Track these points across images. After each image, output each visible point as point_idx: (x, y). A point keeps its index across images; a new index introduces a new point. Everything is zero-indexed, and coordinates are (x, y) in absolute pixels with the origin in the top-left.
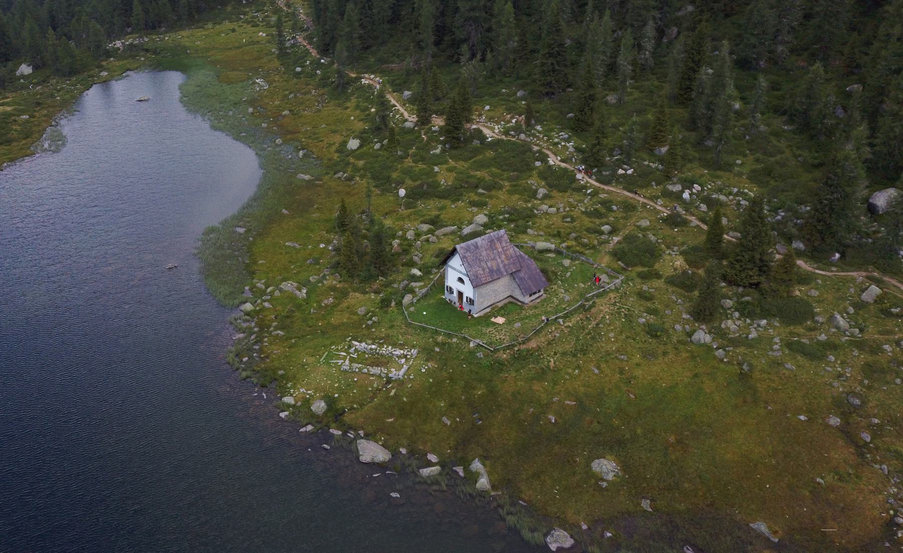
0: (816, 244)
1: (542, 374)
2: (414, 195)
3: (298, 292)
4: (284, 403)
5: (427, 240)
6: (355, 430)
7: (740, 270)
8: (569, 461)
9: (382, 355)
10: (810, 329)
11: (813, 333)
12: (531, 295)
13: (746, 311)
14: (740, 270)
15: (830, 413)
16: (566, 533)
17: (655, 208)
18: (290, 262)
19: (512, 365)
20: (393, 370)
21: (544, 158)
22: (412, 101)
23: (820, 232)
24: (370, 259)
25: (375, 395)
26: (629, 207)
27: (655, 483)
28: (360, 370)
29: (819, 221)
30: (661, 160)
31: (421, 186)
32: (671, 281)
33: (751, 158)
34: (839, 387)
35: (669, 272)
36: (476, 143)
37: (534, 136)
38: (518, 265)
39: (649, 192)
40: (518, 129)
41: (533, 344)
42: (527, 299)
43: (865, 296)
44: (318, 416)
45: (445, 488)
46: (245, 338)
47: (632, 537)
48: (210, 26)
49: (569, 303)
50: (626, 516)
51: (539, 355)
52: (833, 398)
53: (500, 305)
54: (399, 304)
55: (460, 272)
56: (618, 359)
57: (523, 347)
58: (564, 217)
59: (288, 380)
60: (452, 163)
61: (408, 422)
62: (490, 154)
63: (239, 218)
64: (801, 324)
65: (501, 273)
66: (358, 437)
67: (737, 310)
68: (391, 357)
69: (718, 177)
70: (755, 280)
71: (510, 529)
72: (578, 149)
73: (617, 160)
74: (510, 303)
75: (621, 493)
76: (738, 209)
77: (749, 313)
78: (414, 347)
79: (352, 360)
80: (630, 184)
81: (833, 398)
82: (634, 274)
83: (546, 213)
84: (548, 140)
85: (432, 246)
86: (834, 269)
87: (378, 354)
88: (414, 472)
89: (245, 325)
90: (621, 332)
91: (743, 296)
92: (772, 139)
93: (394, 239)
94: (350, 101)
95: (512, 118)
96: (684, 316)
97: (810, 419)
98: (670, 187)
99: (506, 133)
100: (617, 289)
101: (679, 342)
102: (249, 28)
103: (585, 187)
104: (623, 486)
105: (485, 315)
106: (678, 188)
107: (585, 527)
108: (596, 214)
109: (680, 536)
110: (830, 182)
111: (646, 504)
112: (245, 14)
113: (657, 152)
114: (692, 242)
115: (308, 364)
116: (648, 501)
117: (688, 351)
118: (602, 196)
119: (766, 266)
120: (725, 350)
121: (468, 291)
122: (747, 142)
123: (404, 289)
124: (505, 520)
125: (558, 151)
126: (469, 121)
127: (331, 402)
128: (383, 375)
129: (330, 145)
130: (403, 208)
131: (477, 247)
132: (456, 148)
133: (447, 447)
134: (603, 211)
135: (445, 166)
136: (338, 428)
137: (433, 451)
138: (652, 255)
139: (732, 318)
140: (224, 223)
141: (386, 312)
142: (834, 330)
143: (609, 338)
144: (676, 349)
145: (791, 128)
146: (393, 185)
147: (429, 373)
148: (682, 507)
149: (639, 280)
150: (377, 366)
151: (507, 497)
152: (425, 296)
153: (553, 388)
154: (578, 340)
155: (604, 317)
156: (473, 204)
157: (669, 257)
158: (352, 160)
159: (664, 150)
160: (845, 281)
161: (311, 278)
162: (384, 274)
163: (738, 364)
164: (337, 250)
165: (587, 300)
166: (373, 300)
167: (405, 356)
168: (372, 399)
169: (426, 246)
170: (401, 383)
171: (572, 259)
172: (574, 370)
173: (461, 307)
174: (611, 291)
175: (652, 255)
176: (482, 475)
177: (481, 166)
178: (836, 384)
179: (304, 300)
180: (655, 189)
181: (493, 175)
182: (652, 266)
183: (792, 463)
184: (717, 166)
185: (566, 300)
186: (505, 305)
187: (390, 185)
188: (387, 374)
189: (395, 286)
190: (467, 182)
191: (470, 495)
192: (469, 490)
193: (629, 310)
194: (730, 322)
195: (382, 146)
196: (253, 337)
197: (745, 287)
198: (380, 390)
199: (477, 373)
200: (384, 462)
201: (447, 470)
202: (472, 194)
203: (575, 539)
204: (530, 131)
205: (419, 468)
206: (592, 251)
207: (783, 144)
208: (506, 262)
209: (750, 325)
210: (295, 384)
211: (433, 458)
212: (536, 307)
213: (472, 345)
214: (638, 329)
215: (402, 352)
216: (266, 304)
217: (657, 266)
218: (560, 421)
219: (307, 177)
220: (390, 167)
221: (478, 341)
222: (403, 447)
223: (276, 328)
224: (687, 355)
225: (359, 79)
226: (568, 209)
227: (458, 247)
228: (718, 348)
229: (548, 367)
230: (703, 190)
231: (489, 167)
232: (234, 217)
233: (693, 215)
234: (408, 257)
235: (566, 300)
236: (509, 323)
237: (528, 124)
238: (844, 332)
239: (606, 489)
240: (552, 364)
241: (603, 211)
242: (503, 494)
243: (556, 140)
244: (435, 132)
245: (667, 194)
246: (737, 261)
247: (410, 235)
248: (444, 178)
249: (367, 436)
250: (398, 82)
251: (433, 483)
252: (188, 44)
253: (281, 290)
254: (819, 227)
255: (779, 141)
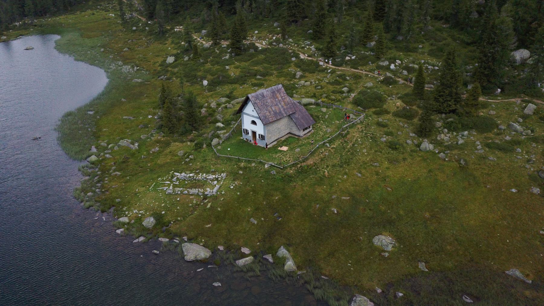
0: (484, 84)
1: (321, 181)
2: (213, 85)
3: (132, 146)
4: (120, 222)
5: (226, 107)
6: (180, 236)
7: (442, 104)
8: (354, 240)
9: (199, 180)
10: (498, 134)
11: (500, 136)
12: (304, 130)
13: (451, 127)
14: (442, 104)
15: (531, 186)
16: (365, 298)
17: (374, 76)
18: (126, 128)
19: (298, 177)
20: (208, 189)
21: (297, 56)
22: (207, 35)
23: (487, 76)
24: (184, 121)
25: (195, 209)
26: (357, 77)
27: (425, 249)
28: (182, 192)
29: (485, 69)
30: (372, 50)
31: (218, 77)
32: (397, 114)
33: (427, 44)
34: (531, 169)
35: (393, 109)
36: (252, 51)
37: (289, 44)
38: (293, 109)
39: (368, 68)
40: (278, 41)
41: (310, 162)
42: (302, 133)
43: (526, 111)
44: (149, 229)
45: (259, 273)
46: (90, 179)
47: (419, 294)
48: (78, 13)
49: (331, 133)
50: (410, 277)
51: (316, 169)
52: (530, 176)
53: (283, 139)
54: (209, 145)
55: (253, 116)
56: (373, 166)
57: (304, 164)
58: (316, 87)
59: (124, 205)
60: (237, 64)
61: (223, 225)
62: (262, 57)
63: (91, 105)
64: (491, 132)
65: (282, 114)
66: (182, 241)
67: (445, 128)
68: (206, 181)
69: (409, 55)
70: (453, 107)
71: (318, 301)
72: (318, 49)
73: (344, 52)
74: (289, 137)
75: (401, 259)
76: (427, 72)
77: (454, 128)
78: (223, 172)
79: (175, 186)
80: (354, 64)
81: (530, 176)
82: (371, 113)
83: (304, 86)
84: (297, 46)
85: (230, 110)
86: (499, 98)
87: (195, 180)
88: (231, 264)
89: (90, 171)
90: (371, 149)
91: (447, 119)
92: (437, 32)
93: (202, 108)
94: (168, 40)
95: (273, 36)
96: (411, 135)
97: (519, 191)
98: (381, 64)
99: (271, 44)
100: (362, 122)
101: (411, 151)
102: (104, 13)
103: (326, 69)
104: (401, 254)
105: (273, 146)
106: (386, 63)
107: (379, 291)
108: (336, 83)
109: (456, 289)
110: (491, 41)
111: (422, 266)
112: (100, 6)
113: (368, 46)
114: (403, 92)
115: (139, 193)
116: (423, 263)
117: (420, 156)
118: (338, 73)
119: (459, 98)
120: (444, 153)
121: (260, 129)
122: (423, 36)
123: (212, 135)
124: (313, 294)
125: (307, 51)
126: (245, 38)
127: (159, 218)
128: (200, 194)
129: (155, 63)
130: (206, 91)
131: (263, 96)
132: (239, 55)
133: (257, 240)
134: (341, 80)
135: (233, 66)
136: (165, 237)
137: (246, 246)
138: (380, 101)
139: (443, 133)
140: (79, 110)
141: (200, 152)
142: (513, 133)
143: (364, 153)
144: (411, 155)
145: (448, 26)
146: (199, 79)
147: (236, 188)
148: (450, 265)
149: (375, 116)
150: (195, 188)
151: (311, 274)
152: (228, 139)
153: (330, 189)
154: (342, 156)
155: (357, 140)
156: (254, 85)
157: (391, 101)
158: (170, 69)
159: (373, 43)
160: (510, 104)
161: (142, 136)
162: (196, 129)
163: (457, 161)
164: (161, 118)
165: (343, 130)
166: (189, 146)
167: (217, 179)
168: (192, 212)
169: (225, 111)
170: (214, 198)
171: (327, 108)
172: (343, 176)
173: (255, 143)
174: (358, 124)
175: (380, 101)
176: (288, 259)
177: (257, 63)
178: (528, 166)
179: (136, 150)
180: (372, 66)
181: (265, 68)
182: (382, 107)
183: (518, 223)
184: (408, 50)
185: (328, 132)
186: (287, 139)
187: (197, 79)
188: (203, 193)
189: (205, 135)
190: (249, 73)
191: (280, 276)
192: (279, 272)
193: (373, 134)
194: (442, 135)
195: (190, 58)
196: (96, 178)
197: (446, 114)
198: (198, 205)
199: (273, 185)
200: (206, 259)
201: (259, 258)
202: (253, 80)
203: (374, 302)
204: (285, 42)
205: (235, 260)
206: (339, 103)
207: (445, 35)
208: (285, 107)
209: (457, 136)
210: (129, 207)
211: (246, 250)
212: (308, 138)
213: (266, 166)
214: (382, 146)
215: (214, 176)
216: (107, 156)
217: (385, 106)
218: (341, 212)
219: (139, 80)
220: (196, 70)
221: (270, 163)
222: (221, 245)
223: (115, 171)
224: (420, 159)
225: (173, 29)
226: (317, 82)
227: (249, 96)
228: (439, 153)
229: (324, 176)
230: (402, 63)
231: (262, 64)
232: (86, 106)
233: (400, 78)
234: (213, 118)
235: (328, 132)
236: (291, 149)
237: (284, 38)
238: (522, 134)
239: (389, 258)
240: (326, 173)
241: (341, 80)
242: (307, 272)
243: (303, 45)
244: (224, 48)
245: (379, 68)
246: (440, 96)
247: (213, 105)
248: (233, 72)
249: (190, 240)
250: (197, 27)
251: (248, 271)
252: (63, 22)
253: (119, 146)
254: (486, 73)
255: (442, 33)
